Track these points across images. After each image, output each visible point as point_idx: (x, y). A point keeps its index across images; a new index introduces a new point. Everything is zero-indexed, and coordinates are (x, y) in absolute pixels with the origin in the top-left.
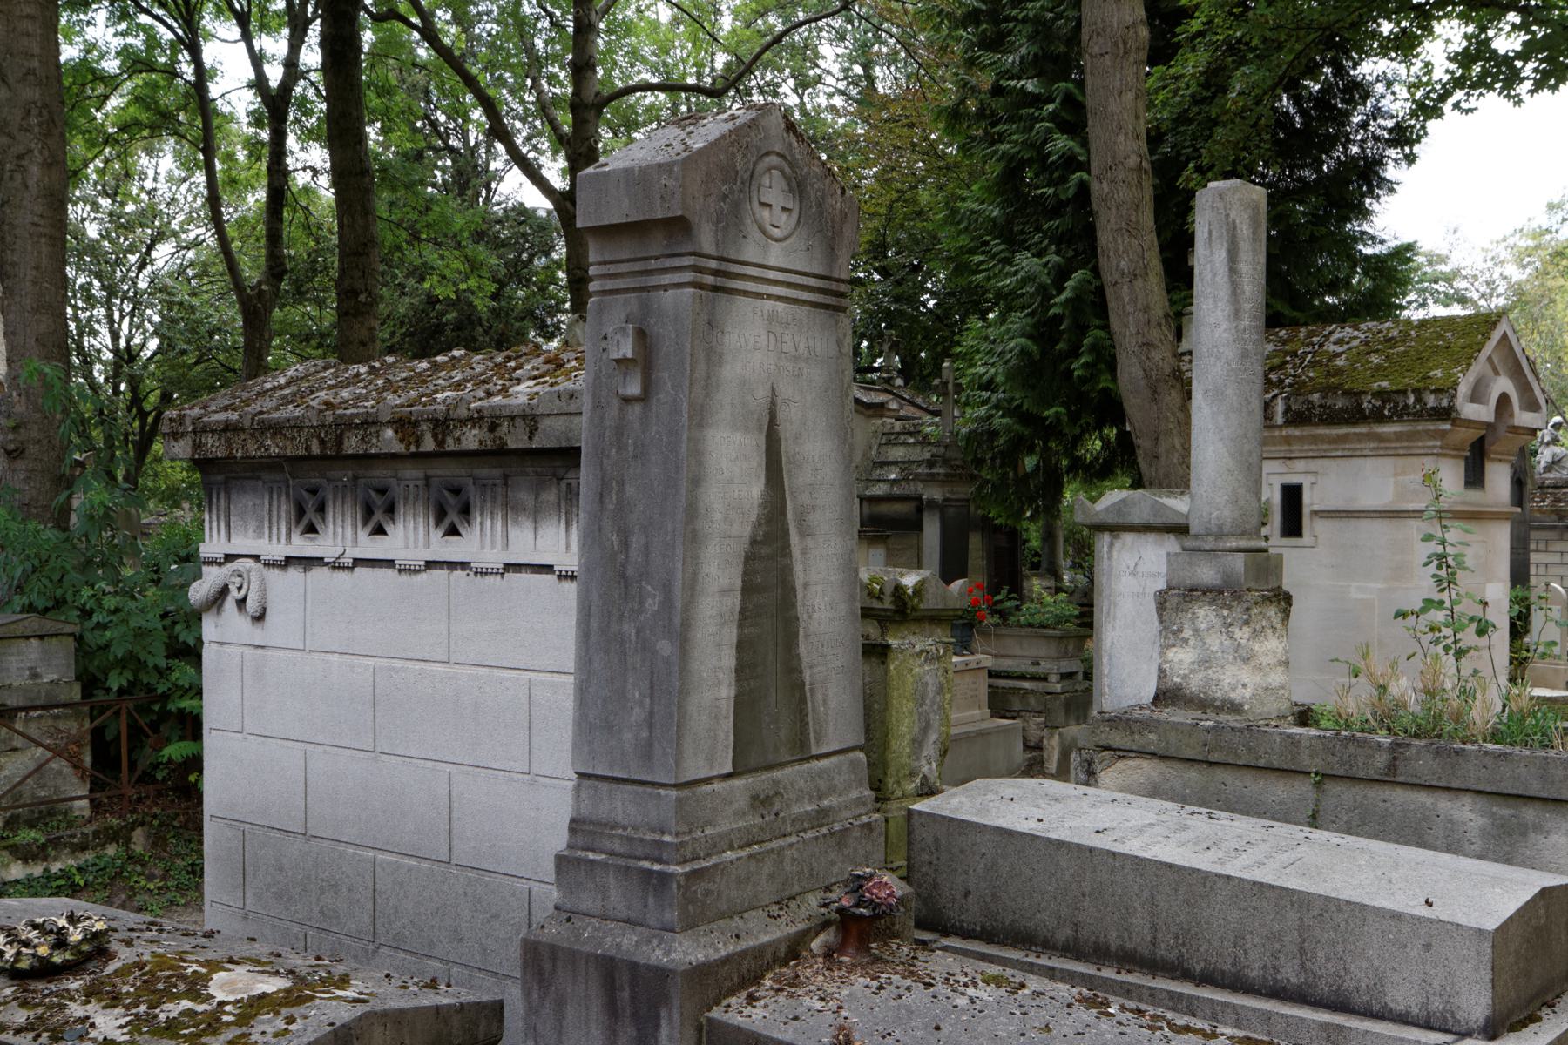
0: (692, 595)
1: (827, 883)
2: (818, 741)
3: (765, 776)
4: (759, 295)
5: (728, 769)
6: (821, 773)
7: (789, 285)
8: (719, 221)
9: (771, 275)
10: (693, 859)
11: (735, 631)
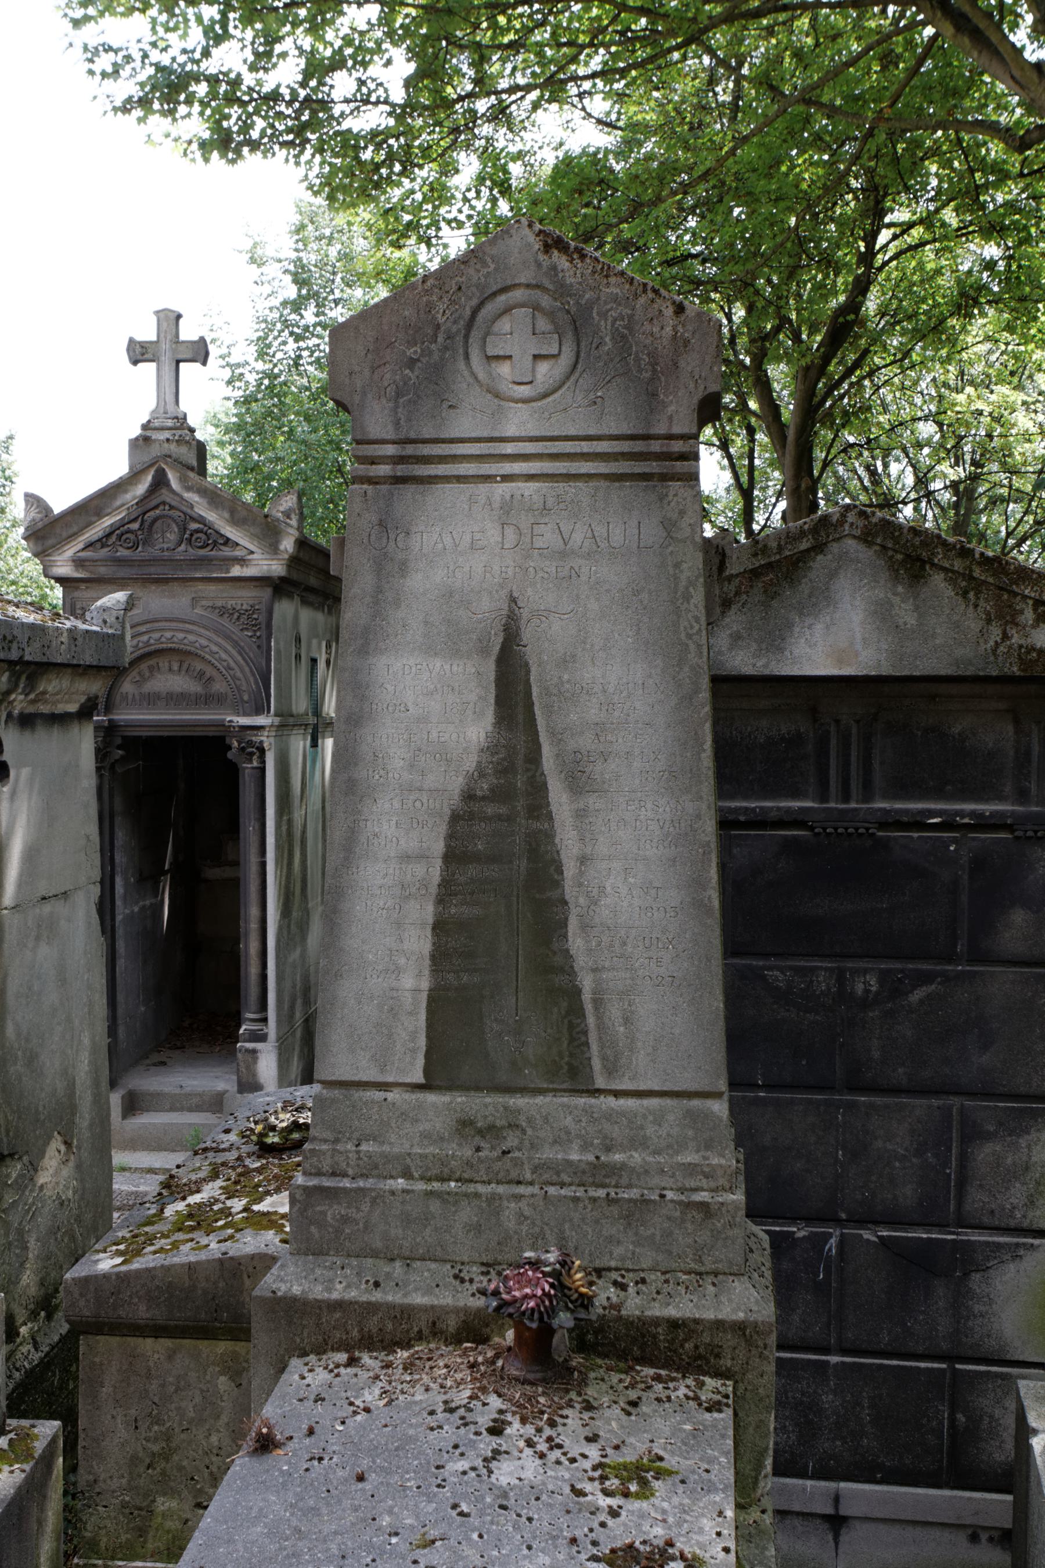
0: (346, 859)
1: (598, 1264)
2: (611, 1070)
3: (500, 1099)
4: (487, 478)
5: (418, 1077)
6: (610, 1116)
7: (454, 458)
8: (399, 394)
9: (509, 448)
10: (334, 1174)
11: (430, 908)
